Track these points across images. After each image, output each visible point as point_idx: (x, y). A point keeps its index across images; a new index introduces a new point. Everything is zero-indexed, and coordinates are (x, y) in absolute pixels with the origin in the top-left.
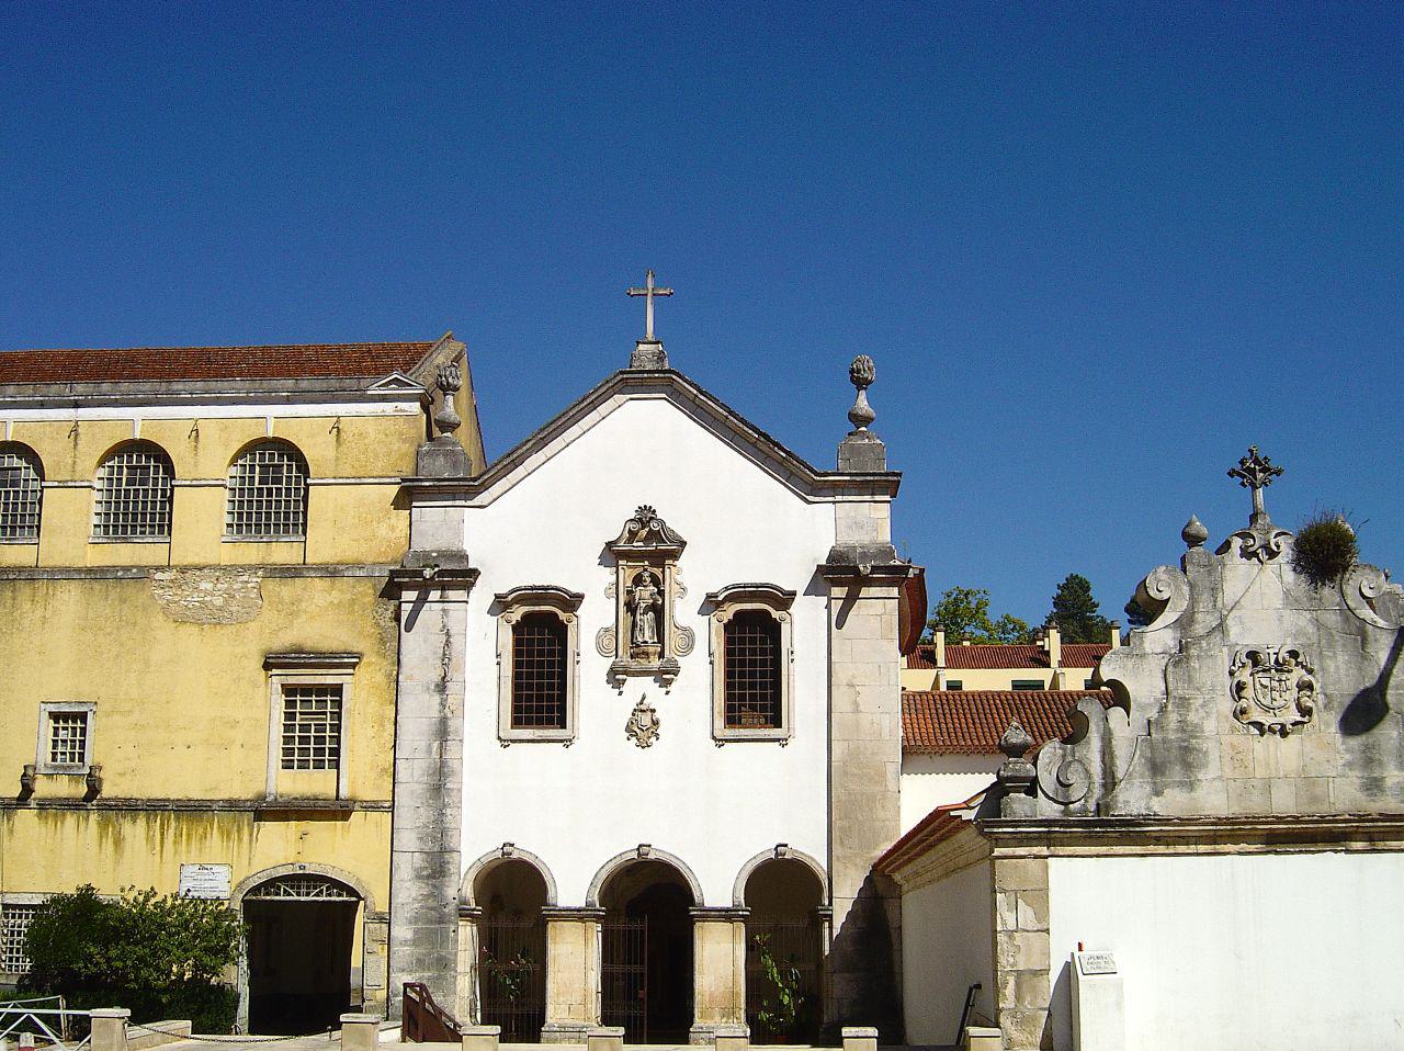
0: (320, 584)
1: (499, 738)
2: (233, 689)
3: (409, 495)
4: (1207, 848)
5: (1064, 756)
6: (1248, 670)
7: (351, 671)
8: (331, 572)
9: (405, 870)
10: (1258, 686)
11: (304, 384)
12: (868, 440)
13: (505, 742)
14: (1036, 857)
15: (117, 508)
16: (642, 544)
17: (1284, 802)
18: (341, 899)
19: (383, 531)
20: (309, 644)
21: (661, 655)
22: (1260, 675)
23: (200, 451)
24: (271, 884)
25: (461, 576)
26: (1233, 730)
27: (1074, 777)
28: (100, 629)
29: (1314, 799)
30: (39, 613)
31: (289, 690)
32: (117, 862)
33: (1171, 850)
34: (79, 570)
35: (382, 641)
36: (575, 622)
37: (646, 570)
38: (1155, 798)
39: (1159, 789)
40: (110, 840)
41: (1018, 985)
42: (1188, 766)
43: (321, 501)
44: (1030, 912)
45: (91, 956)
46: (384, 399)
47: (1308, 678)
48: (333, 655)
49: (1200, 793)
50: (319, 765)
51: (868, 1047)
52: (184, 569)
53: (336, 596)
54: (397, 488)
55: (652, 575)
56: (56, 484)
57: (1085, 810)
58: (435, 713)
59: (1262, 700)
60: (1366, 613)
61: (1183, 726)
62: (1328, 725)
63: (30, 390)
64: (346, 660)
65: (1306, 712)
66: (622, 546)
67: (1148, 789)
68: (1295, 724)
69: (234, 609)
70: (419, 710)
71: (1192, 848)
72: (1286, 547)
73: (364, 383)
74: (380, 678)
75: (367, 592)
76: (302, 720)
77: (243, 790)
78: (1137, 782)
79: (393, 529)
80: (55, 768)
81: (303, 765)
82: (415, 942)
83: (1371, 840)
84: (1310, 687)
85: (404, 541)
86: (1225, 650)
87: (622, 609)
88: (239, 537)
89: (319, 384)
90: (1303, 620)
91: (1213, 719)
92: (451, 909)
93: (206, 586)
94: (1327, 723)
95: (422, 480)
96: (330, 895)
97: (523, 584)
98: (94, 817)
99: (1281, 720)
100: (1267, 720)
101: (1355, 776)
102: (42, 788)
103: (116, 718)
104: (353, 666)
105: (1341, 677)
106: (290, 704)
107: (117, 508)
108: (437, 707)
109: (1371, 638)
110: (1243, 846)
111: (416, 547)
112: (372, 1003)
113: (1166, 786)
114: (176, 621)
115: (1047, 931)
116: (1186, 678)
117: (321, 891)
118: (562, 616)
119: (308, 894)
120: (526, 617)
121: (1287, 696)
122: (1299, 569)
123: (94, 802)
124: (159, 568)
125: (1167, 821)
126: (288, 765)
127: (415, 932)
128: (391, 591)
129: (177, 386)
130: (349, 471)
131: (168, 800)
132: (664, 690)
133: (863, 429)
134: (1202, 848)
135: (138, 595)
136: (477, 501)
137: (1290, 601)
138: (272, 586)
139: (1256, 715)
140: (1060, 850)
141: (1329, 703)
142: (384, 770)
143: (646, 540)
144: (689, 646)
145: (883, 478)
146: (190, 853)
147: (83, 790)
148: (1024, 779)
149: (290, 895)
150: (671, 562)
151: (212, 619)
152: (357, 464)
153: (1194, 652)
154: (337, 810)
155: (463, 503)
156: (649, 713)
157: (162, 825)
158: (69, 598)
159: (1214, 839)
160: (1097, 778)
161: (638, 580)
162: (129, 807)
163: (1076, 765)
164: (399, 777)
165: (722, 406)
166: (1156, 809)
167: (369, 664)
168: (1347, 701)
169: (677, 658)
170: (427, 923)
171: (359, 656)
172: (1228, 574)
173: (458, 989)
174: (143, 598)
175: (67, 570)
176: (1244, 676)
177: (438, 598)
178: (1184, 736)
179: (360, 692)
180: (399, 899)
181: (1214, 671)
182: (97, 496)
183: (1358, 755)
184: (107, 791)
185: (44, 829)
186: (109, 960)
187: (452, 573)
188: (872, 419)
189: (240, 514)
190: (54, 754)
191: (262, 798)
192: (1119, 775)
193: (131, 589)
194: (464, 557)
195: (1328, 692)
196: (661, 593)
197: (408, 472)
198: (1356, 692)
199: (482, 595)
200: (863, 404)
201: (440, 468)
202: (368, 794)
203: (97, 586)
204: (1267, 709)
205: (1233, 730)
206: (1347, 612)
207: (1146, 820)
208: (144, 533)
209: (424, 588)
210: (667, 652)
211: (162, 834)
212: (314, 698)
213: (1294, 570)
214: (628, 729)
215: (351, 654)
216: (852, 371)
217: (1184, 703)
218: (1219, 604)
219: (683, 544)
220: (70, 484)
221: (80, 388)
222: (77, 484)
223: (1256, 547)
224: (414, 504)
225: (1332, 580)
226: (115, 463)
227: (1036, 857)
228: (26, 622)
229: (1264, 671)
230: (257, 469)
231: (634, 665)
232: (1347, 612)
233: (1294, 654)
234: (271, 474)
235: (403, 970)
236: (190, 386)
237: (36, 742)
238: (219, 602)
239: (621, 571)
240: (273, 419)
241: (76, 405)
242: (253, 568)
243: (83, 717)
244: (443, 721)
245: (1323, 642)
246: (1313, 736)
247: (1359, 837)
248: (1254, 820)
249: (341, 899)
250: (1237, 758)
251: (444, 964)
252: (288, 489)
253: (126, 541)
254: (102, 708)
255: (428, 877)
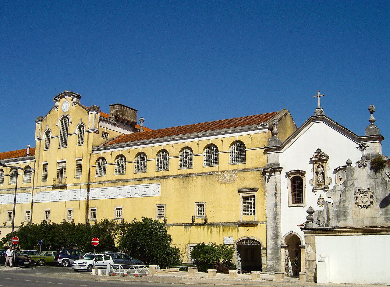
0: (249, 173)
1: (289, 206)
2: (232, 198)
3: (267, 151)
4: (350, 234)
5: (319, 214)
6: (359, 193)
7: (256, 192)
8: (251, 170)
9: (269, 238)
10: (361, 197)
11: (243, 128)
12: (373, 126)
13: (290, 207)
14: (313, 236)
15: (208, 159)
16: (318, 158)
17: (366, 223)
18: (256, 244)
19: (262, 160)
20: (247, 187)
21: (324, 185)
22: (361, 194)
23: (223, 145)
24: (242, 241)
25: (278, 169)
26: (355, 207)
27: (321, 218)
28: (206, 186)
29: (373, 223)
30: (194, 183)
31: (244, 197)
32: (211, 236)
33: (341, 234)
34: (201, 173)
35: (263, 185)
36: (304, 178)
37: (320, 164)
38: (338, 223)
39: (339, 221)
40: (210, 233)
41: (309, 263)
42: (345, 216)
43: (249, 154)
44: (311, 248)
45: (201, 257)
46: (260, 129)
47: (372, 194)
48: (250, 189)
49: (348, 221)
50: (251, 214)
51: (280, 276)
52: (221, 172)
53: (252, 175)
54: (264, 149)
55: (322, 165)
56: (196, 155)
57: (323, 226)
58: (274, 201)
59: (362, 200)
60: (387, 178)
61: (344, 206)
62: (377, 205)
63: (189, 135)
64: (255, 190)
65: (371, 202)
66: (314, 159)
67: (336, 221)
68: (369, 205)
69: (232, 180)
70: (271, 200)
71: (346, 234)
72: (368, 164)
73: (256, 126)
74: (262, 194)
75: (259, 174)
76: (247, 204)
77: (235, 220)
78: (334, 219)
79: (264, 159)
80: (198, 216)
81: (248, 214)
82: (272, 254)
83: (387, 232)
84: (373, 196)
85: (266, 162)
86: (354, 189)
87: (315, 174)
88: (232, 164)
89: (246, 127)
90: (372, 181)
91: (351, 205)
92: (279, 246)
93: (226, 175)
94: (377, 205)
95: (269, 147)
96: (254, 243)
97: (292, 170)
98: (206, 227)
99: (365, 204)
100: (362, 205)
101: (383, 217)
102: (196, 221)
103: (210, 205)
104: (257, 191)
105: (381, 194)
106: (244, 200)
107: (208, 159)
108: (275, 200)
109: (388, 184)
110: (358, 234)
111: (269, 163)
112: (263, 268)
113: (340, 220)
114: (220, 183)
115: (315, 252)
116: (345, 196)
117: (252, 242)
118: (301, 177)
119: (250, 243)
120: (294, 177)
121: (367, 199)
122: (371, 169)
123: (206, 224)
124: (216, 172)
125: (339, 228)
126: (245, 214)
127: (272, 251)
128: (264, 174)
129: (218, 131)
130: (253, 146)
131: (221, 223)
132: (315, 194)
133: (372, 124)
134: (348, 234)
135: (213, 178)
136: (281, 151)
137: (369, 177)
138: (239, 174)
139: (361, 204)
140: (318, 235)
141: (377, 200)
142: (265, 215)
143: (319, 157)
144: (331, 182)
145: (375, 136)
146: (225, 234)
147: (204, 221)
148: (311, 219)
149: (246, 243)
150: (326, 162)
151: (227, 182)
152: (255, 145)
153: (347, 190)
154: (255, 224)
155: (278, 152)
156: (322, 199)
157: (220, 228)
158: (199, 179)
159: (351, 232)
160: (326, 219)
161: (318, 167)
162: (213, 225)
163: (321, 216)
164: (267, 216)
165: (335, 122)
166: (338, 225)
167: (260, 190)
168: (382, 200)
169: (328, 185)
170: (274, 250)
171: (258, 189)
172: (355, 172)
173: (282, 264)
174: (213, 179)
175: (199, 174)
176: (358, 195)
177: (273, 174)
178: (344, 209)
179: (258, 197)
180: (268, 244)
181: (351, 194)
182: (204, 157)
183: (384, 212)
184: (209, 221)
185: (197, 230)
186: (204, 258)
187: (276, 168)
188: (375, 121)
189: (233, 158)
190: (198, 214)
191: (239, 222)
192: (330, 218)
193: (211, 177)
194: (279, 164)
195: (377, 198)
196: (324, 170)
197: (266, 146)
198: (384, 197)
199: (283, 173)
200: (372, 117)
201: (273, 144)
202: (261, 220)
203: (204, 176)
204: (363, 202)
205: (355, 207)
206: (383, 179)
207: (335, 228)
208: (213, 164)
209: (270, 172)
210: (325, 184)
211: (220, 230)
212: (246, 199)
213: (370, 169)
214: (317, 203)
215: (256, 188)
216: (369, 109)
217: (344, 201)
218: (353, 179)
219: (328, 157)
220: (198, 155)
221: (199, 133)
222: (200, 155)
223: (361, 165)
224: (268, 153)
225: (379, 171)
226: (207, 149)
227: (313, 236)
228: (191, 185)
229: (362, 193)
230: (235, 148)
231: (318, 187)
232: (383, 179)
233: (369, 189)
234: (238, 148)
235: (270, 260)
236: (220, 130)
237: (195, 212)
238: (229, 178)
239: (314, 165)
240: (237, 136)
241: (198, 137)
242: (235, 170)
243: (203, 205)
244: (276, 203)
245: (376, 186)
246: (373, 208)
247: (384, 231)
248: (358, 228)
249: (256, 244)
250: (356, 213)
251: (278, 259)
252: (242, 152)
253: (210, 166)
254: (206, 203)
255: (274, 239)
